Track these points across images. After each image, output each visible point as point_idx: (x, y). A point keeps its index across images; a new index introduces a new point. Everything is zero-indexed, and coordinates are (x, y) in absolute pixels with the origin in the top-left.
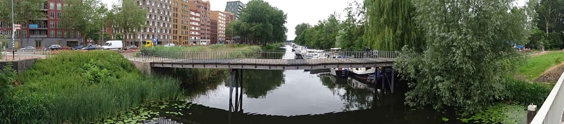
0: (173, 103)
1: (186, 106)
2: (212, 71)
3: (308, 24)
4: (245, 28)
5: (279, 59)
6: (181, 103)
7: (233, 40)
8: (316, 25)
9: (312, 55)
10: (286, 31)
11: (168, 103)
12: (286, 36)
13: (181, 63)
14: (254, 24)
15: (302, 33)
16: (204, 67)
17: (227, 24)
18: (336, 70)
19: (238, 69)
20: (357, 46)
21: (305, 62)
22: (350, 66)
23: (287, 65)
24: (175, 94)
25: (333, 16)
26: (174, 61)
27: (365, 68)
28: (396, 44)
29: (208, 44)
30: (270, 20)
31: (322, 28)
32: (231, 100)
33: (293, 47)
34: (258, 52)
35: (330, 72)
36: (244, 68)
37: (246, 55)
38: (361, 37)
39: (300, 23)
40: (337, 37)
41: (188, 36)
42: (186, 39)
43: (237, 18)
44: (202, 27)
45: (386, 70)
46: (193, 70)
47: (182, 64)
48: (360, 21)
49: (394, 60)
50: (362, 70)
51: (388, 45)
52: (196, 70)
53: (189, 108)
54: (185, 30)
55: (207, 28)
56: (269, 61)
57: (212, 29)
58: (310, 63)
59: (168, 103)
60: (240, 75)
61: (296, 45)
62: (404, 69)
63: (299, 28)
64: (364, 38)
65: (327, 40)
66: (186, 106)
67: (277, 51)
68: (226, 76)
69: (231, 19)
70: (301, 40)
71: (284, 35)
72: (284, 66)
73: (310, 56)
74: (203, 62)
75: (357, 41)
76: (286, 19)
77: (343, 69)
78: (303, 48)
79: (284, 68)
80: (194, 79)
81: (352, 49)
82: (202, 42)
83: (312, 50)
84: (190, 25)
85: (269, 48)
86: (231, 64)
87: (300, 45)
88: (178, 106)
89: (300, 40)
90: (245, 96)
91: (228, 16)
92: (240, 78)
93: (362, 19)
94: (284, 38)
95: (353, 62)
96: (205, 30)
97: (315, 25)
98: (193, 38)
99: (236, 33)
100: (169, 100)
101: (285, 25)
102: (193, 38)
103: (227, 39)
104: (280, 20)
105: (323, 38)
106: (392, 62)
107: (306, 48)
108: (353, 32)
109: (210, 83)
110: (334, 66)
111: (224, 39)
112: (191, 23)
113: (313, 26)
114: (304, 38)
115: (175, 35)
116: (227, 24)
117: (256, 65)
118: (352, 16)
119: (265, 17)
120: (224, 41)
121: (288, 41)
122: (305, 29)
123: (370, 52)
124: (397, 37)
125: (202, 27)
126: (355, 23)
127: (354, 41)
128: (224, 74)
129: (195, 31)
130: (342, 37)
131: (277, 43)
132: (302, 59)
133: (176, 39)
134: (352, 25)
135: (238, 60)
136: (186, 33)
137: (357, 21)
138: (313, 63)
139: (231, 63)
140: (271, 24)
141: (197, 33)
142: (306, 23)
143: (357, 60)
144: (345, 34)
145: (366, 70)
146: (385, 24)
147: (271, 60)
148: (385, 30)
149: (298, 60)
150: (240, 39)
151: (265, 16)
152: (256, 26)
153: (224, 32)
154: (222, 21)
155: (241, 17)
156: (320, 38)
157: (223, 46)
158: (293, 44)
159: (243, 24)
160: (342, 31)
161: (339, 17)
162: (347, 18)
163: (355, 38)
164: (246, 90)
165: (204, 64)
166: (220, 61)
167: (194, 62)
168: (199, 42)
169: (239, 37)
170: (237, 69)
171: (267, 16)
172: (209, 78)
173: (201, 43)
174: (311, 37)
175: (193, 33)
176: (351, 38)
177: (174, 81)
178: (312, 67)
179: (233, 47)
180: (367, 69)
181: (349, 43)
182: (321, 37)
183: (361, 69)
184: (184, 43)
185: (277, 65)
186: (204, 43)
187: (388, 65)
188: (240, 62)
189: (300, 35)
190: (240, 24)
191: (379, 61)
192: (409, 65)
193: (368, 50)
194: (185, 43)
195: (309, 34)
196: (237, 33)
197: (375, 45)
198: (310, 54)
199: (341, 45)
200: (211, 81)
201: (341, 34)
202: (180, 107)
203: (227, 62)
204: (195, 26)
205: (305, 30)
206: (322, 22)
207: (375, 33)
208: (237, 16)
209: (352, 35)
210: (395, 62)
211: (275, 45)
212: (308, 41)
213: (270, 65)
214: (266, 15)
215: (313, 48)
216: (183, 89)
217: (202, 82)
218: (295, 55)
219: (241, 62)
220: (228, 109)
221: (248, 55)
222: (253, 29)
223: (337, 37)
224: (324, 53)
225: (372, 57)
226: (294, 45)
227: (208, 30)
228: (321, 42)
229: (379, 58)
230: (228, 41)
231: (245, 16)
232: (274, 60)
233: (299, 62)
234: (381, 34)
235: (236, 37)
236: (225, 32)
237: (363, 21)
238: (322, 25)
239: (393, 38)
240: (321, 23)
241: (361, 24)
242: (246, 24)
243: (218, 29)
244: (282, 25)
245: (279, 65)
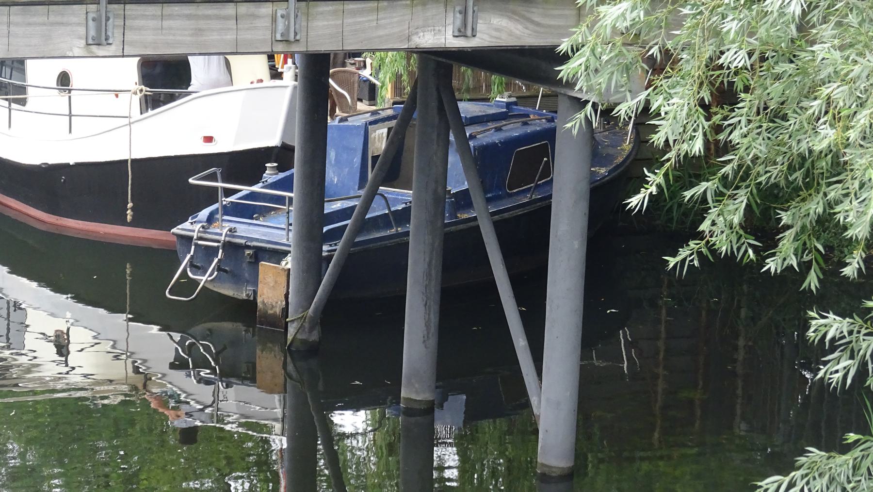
32: (287, 296)
45: (467, 109)
62: (747, 102)
183: (64, 80)
192: (827, 31)
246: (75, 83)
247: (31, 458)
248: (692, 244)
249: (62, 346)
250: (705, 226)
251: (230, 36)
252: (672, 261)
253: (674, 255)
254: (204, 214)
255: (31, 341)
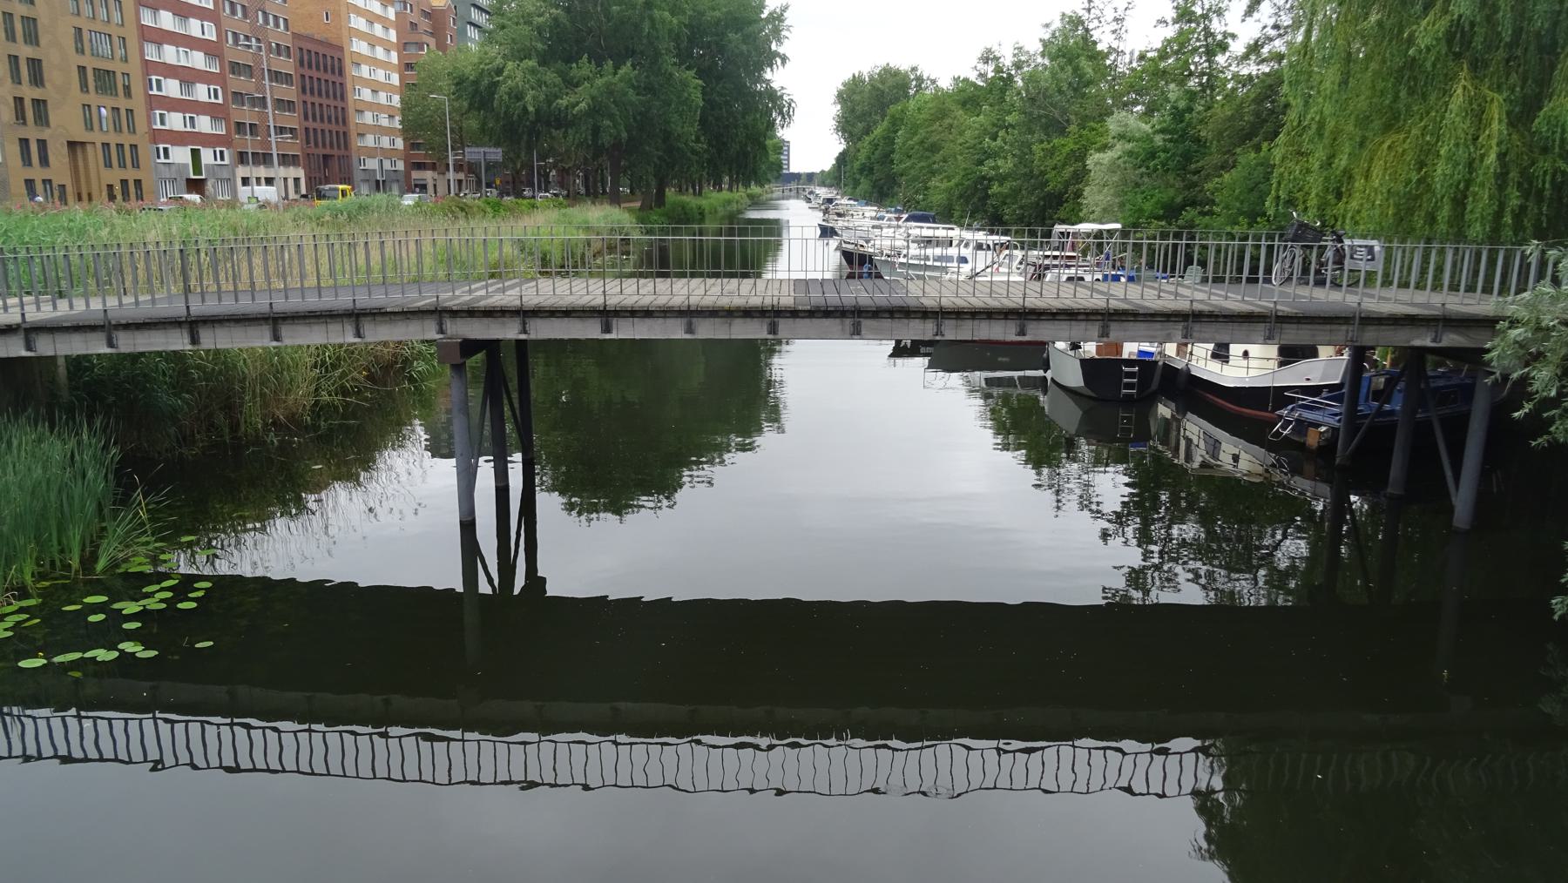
0: (71, 592)
1: (169, 595)
2: (334, 367)
3: (914, 69)
4: (528, 98)
5: (745, 276)
6: (135, 584)
7: (459, 167)
8: (966, 80)
9: (939, 259)
10: (781, 113)
11: (32, 602)
12: (782, 147)
13: (98, 319)
14: (583, 68)
15: (878, 131)
16: (276, 338)
17: (409, 66)
18: (1087, 356)
19: (498, 341)
20: (1227, 207)
21: (897, 298)
22: (1178, 329)
23: (794, 313)
24: (75, 537)
25: (1076, 22)
26: (42, 311)
27: (1272, 351)
28: (1526, 195)
29: (292, 195)
30: (684, 45)
31: (1002, 100)
32: (468, 527)
33: (826, 212)
34: (618, 246)
35: (1046, 367)
36: (533, 336)
37: (545, 261)
38: (1258, 149)
39: (867, 64)
40: (1097, 156)
41: (141, 138)
42: (122, 165)
43: (472, 33)
44: (240, 83)
46: (198, 367)
47: (107, 328)
48: (1254, 48)
49: (1511, 310)
50: (1253, 363)
51: (1459, 202)
52: (222, 374)
53: (193, 605)
54: (110, 101)
55: (272, 91)
56: (685, 291)
57: (309, 99)
58: (929, 303)
59: (32, 602)
60: (513, 385)
61: (845, 201)
63: (857, 98)
64: (1278, 154)
65: (1030, 175)
66: (169, 595)
67: (731, 232)
68: (430, 390)
69: (437, 32)
70: (871, 170)
71: (769, 142)
72: (772, 315)
73: (927, 267)
74: (266, 309)
75: (1226, 176)
76: (779, 41)
77: (1130, 349)
78: (882, 218)
79: (773, 329)
80: (212, 425)
81: (1191, 224)
82: (245, 181)
83: (941, 232)
84: (149, 67)
85: (683, 217)
86: (454, 314)
87: (868, 199)
88: (116, 606)
89: (867, 170)
90: (549, 504)
91: (414, 17)
92: (515, 396)
93: (1273, 33)
94: (772, 158)
95: (1198, 307)
96: (265, 107)
97: (956, 79)
98: (180, 155)
99: (473, 123)
100: (42, 577)
101: (777, 77)
102: (180, 155)
103: (420, 166)
104: (744, 48)
105: (1006, 165)
106: (1488, 324)
107: (905, 216)
108: (1201, 121)
109: (326, 439)
110: (1077, 329)
111: (400, 166)
112: (151, 53)
113: (945, 83)
114: (887, 159)
115: (33, 133)
116: (409, 66)
117: (606, 315)
118: (1205, 17)
119: (653, 26)
120: (402, 179)
121: (797, 177)
122: (896, 100)
123: (1322, 249)
124: (1545, 150)
125: (240, 83)
126: (1221, 59)
127: (1208, 177)
128: (411, 380)
129: (190, 107)
130: (1130, 153)
131: (730, 189)
132: (878, 281)
133: (44, 161)
134: (1203, 74)
135: (498, 290)
136: (124, 119)
137: (1237, 48)
138: (945, 303)
139: (452, 304)
140: (688, 68)
141: (204, 124)
142: (904, 66)
143: (1226, 298)
144: (1148, 138)
145: (1281, 364)
146: (1458, 56)
147: (695, 282)
148: (1446, 104)
149: (855, 285)
150: (504, 165)
151: (652, 20)
152: (599, 82)
153: (391, 117)
154: (373, 46)
155: (503, 27)
156: (990, 163)
157: (393, 208)
158: (823, 192)
159: (516, 74)
160: (1131, 120)
161: (1114, 26)
162: (1170, 31)
163: (1215, 158)
164: (555, 468)
165: (275, 321)
166: (378, 299)
167: (198, 308)
168: (230, 181)
169: (496, 154)
170: (491, 346)
171: (663, 21)
172: (318, 409)
173: (243, 192)
174: (934, 148)
175: (175, 121)
176: (1187, 157)
177: (56, 449)
178: (939, 326)
179: (461, 215)
180: (1290, 355)
181: (1171, 192)
182: (993, 155)
183: (1246, 354)
184: (110, 187)
185: (729, 314)
186: (264, 187)
187: (1451, 339)
188: (509, 296)
189: (867, 139)
190: (499, 71)
191: (1387, 308)
193: (1303, 233)
194: (118, 188)
195: (922, 132)
196: (483, 129)
197: (1354, 204)
198: (929, 251)
199: (1122, 205)
200: (330, 430)
201: (1121, 137)
202: (131, 608)
203: (426, 300)
204: (188, 77)
205: (894, 109)
206: (1007, 61)
207: (1364, 121)
208: (475, 15)
209: (1197, 140)
210: (1514, 323)
211: (715, 198)
212: (915, 179)
213: (689, 314)
214: (657, 13)
215: (946, 216)
216: (138, 495)
217: (273, 439)
218: (835, 258)
219: (518, 303)
220: (449, 577)
221: (556, 257)
222: (578, 101)
223: (1095, 159)
224: (1018, 254)
225: (1336, 285)
226: (830, 201)
227: (280, 104)
228: (995, 188)
229: (1386, 293)
230: (428, 175)
231: (528, 23)
232: (710, 281)
233: (860, 293)
234: (1415, 131)
235: (473, 153)
236: (398, 118)
237: (1279, 45)
238: (1000, 85)
239: (1501, 156)
240: (998, 70)
241: (1265, 68)
242: (533, 71)
243: (352, 98)
244: (760, 79)
245: (748, 313)
246: (1250, 355)
247: (1314, 503)
248: (1545, 437)
249: (1236, 458)
250: (1552, 429)
251: (1328, 338)
252: (1534, 443)
253: (1535, 440)
254: (1290, 407)
255: (1222, 456)
